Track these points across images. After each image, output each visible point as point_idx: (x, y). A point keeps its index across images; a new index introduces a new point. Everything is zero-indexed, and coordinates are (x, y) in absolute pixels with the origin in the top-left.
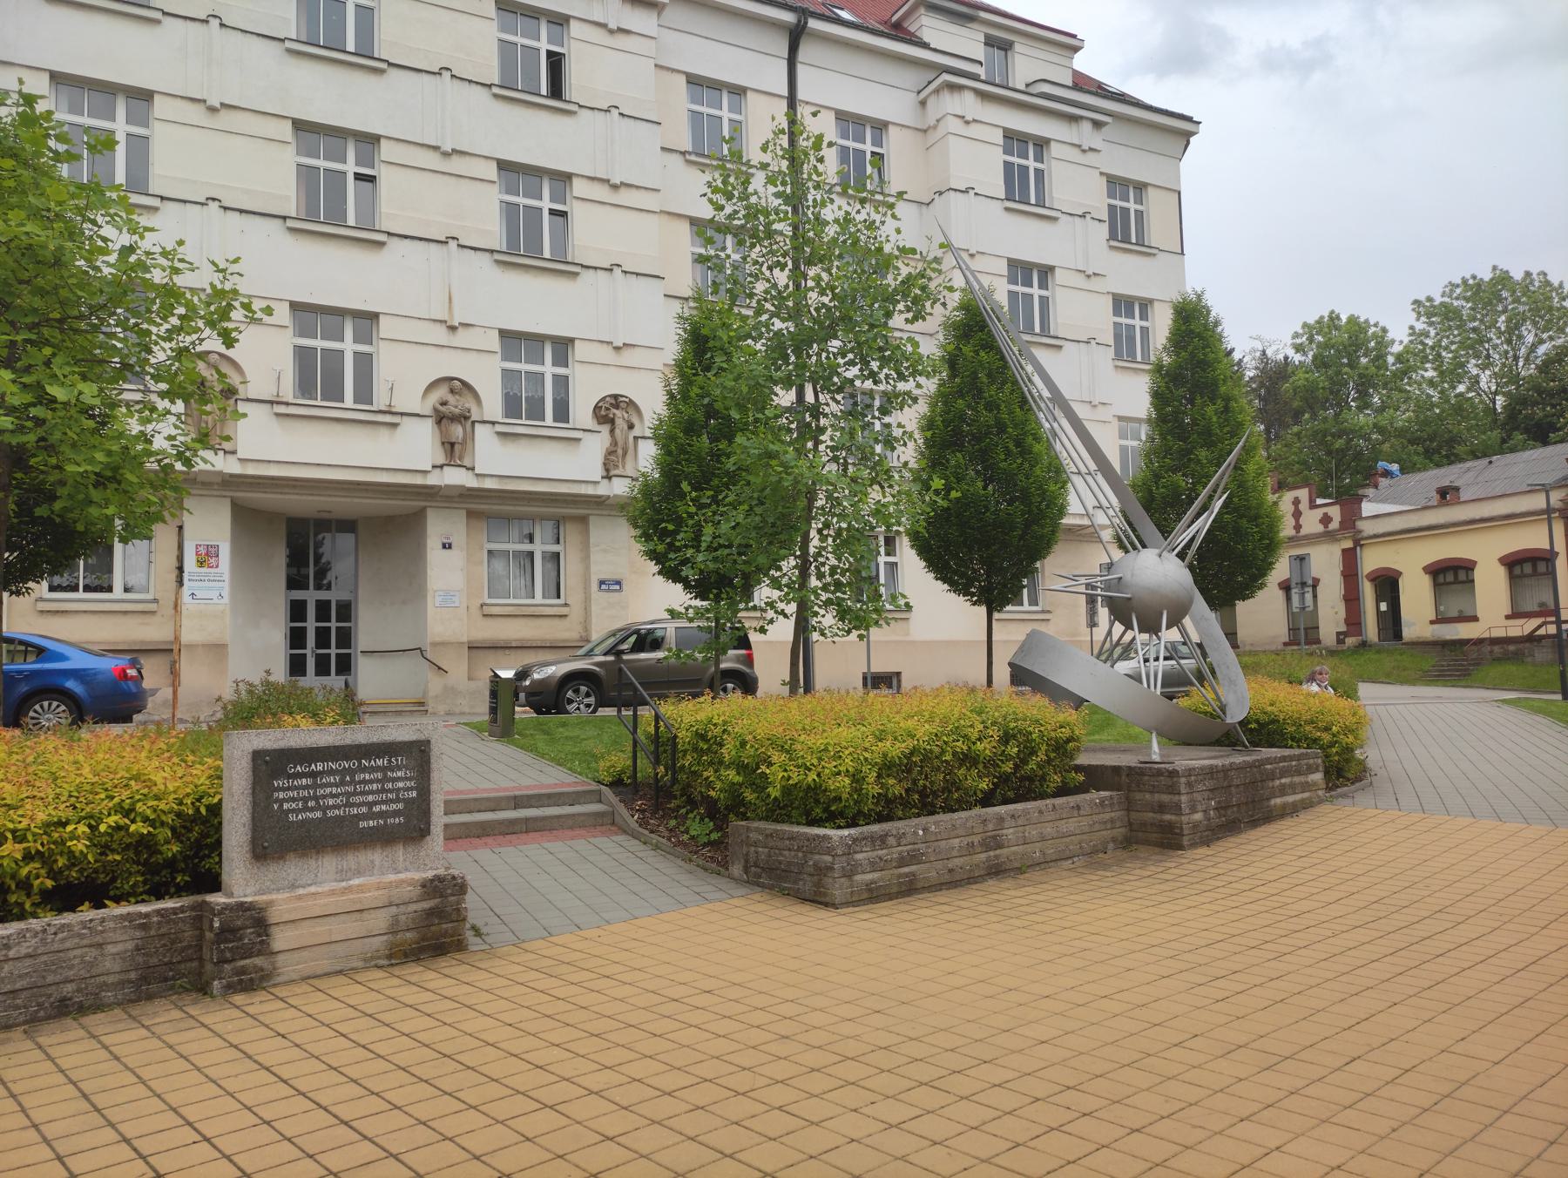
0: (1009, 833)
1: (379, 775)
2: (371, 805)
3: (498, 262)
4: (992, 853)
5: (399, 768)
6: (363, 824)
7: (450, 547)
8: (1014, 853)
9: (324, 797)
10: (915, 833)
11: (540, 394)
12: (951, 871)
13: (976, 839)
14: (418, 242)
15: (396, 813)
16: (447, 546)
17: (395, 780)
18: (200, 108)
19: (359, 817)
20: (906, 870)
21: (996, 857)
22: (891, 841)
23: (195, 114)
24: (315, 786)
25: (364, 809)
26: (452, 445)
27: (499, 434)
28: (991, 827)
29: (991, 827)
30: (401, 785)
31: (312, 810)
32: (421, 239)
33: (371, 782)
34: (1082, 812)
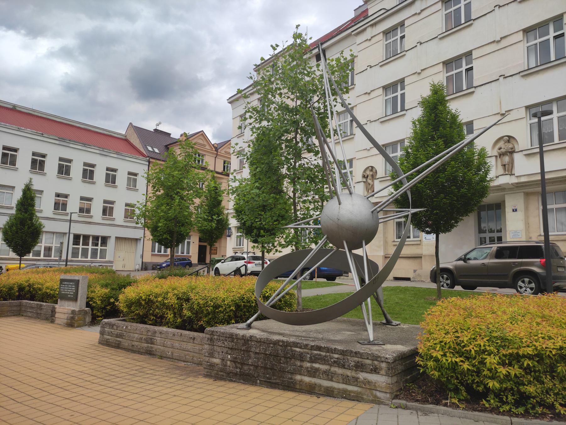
0: (158, 339)
3: (523, 76)
4: (150, 345)
7: (516, 210)
8: (159, 349)
10: (123, 327)
11: (552, 130)
12: (133, 346)
13: (144, 337)
14: (488, 84)
16: (515, 210)
18: (416, 75)
20: (118, 339)
21: (152, 348)
22: (115, 327)
23: (415, 78)
26: (505, 165)
27: (526, 155)
28: (150, 334)
29: (150, 334)
32: (488, 83)
34: (195, 342)
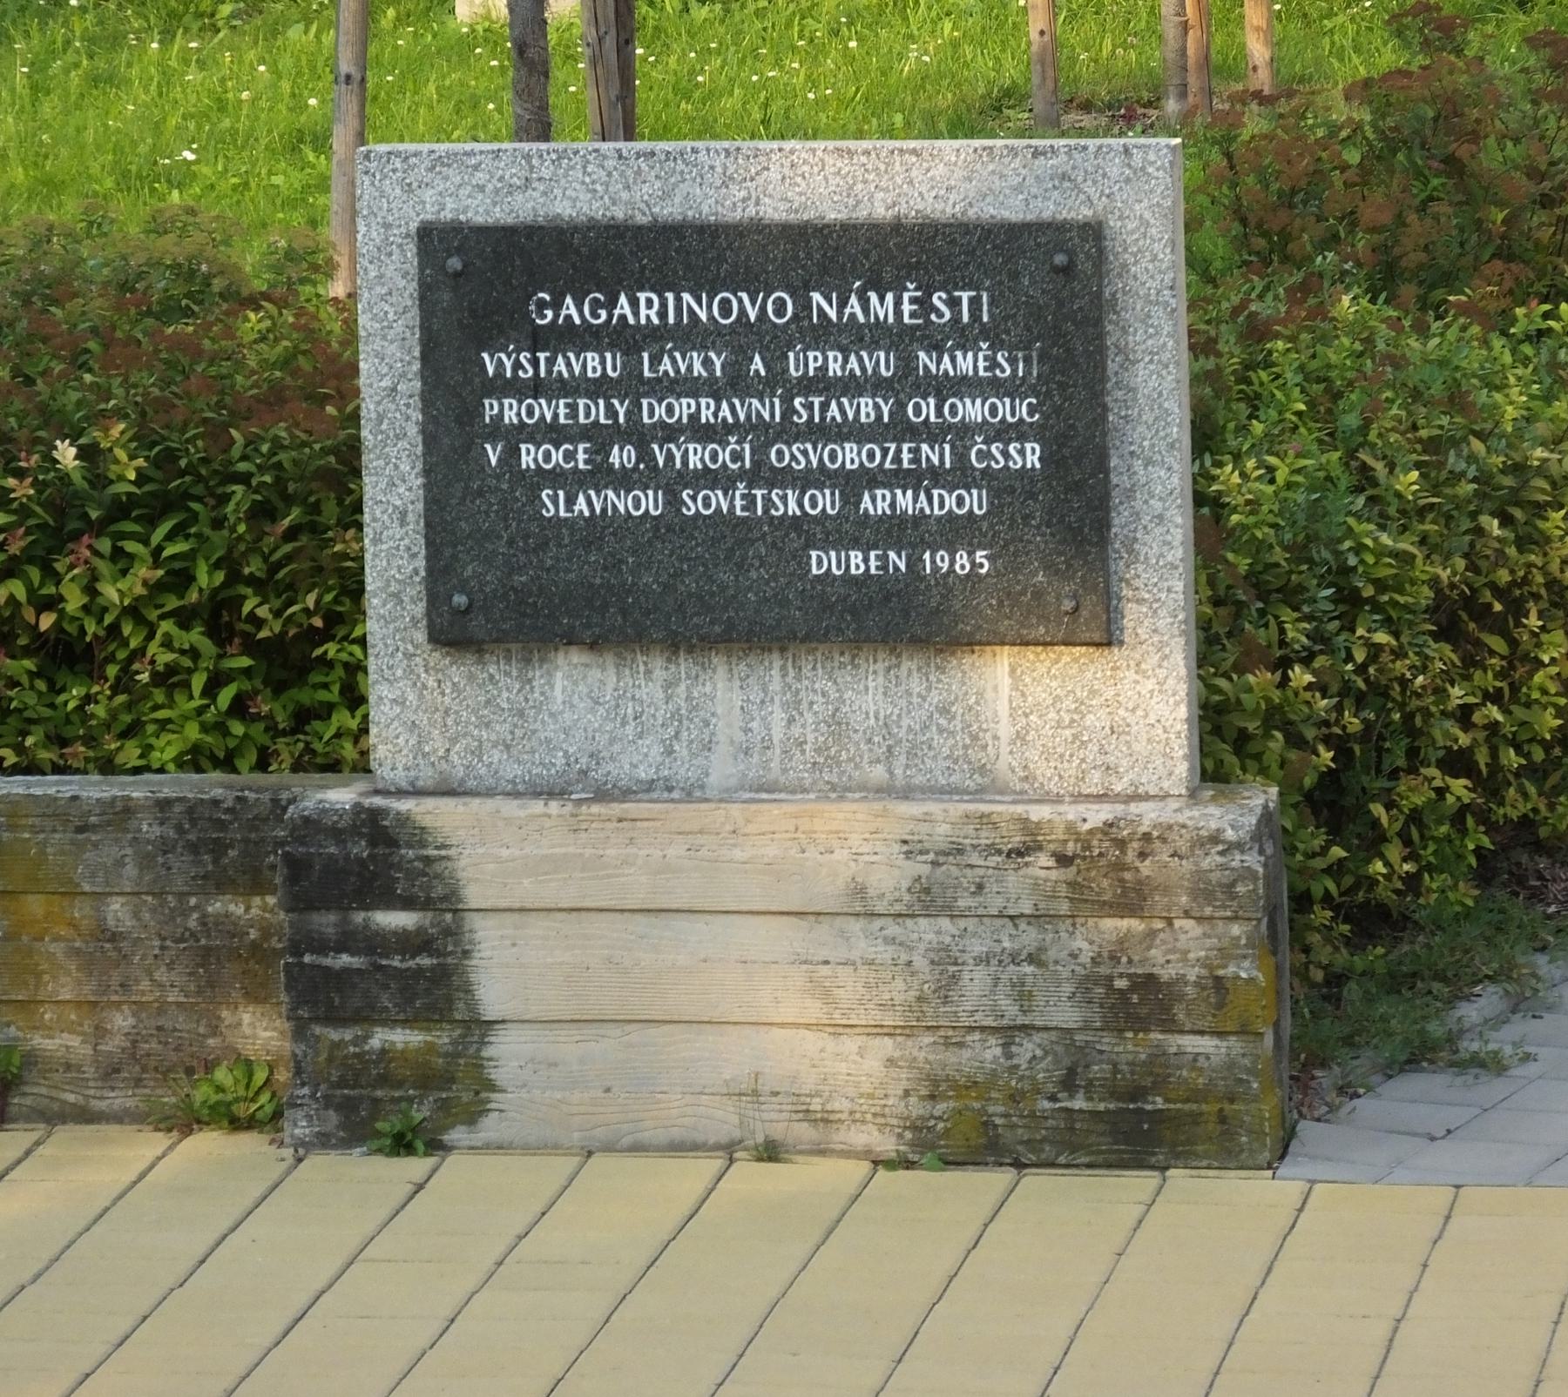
1: (883, 363)
2: (852, 484)
5: (964, 337)
6: (821, 562)
9: (670, 433)
15: (956, 531)
17: (946, 388)
19: (809, 532)
24: (632, 386)
25: (826, 502)
30: (973, 410)
31: (624, 481)
33: (851, 386)
